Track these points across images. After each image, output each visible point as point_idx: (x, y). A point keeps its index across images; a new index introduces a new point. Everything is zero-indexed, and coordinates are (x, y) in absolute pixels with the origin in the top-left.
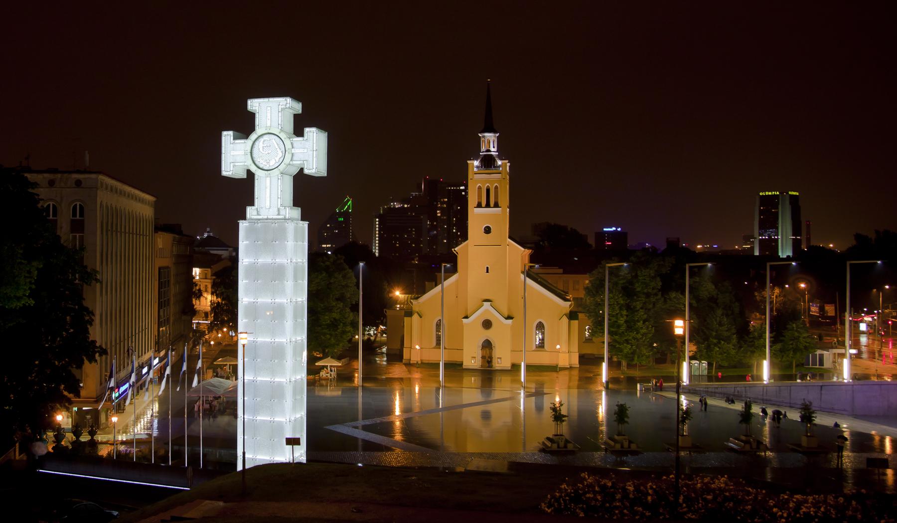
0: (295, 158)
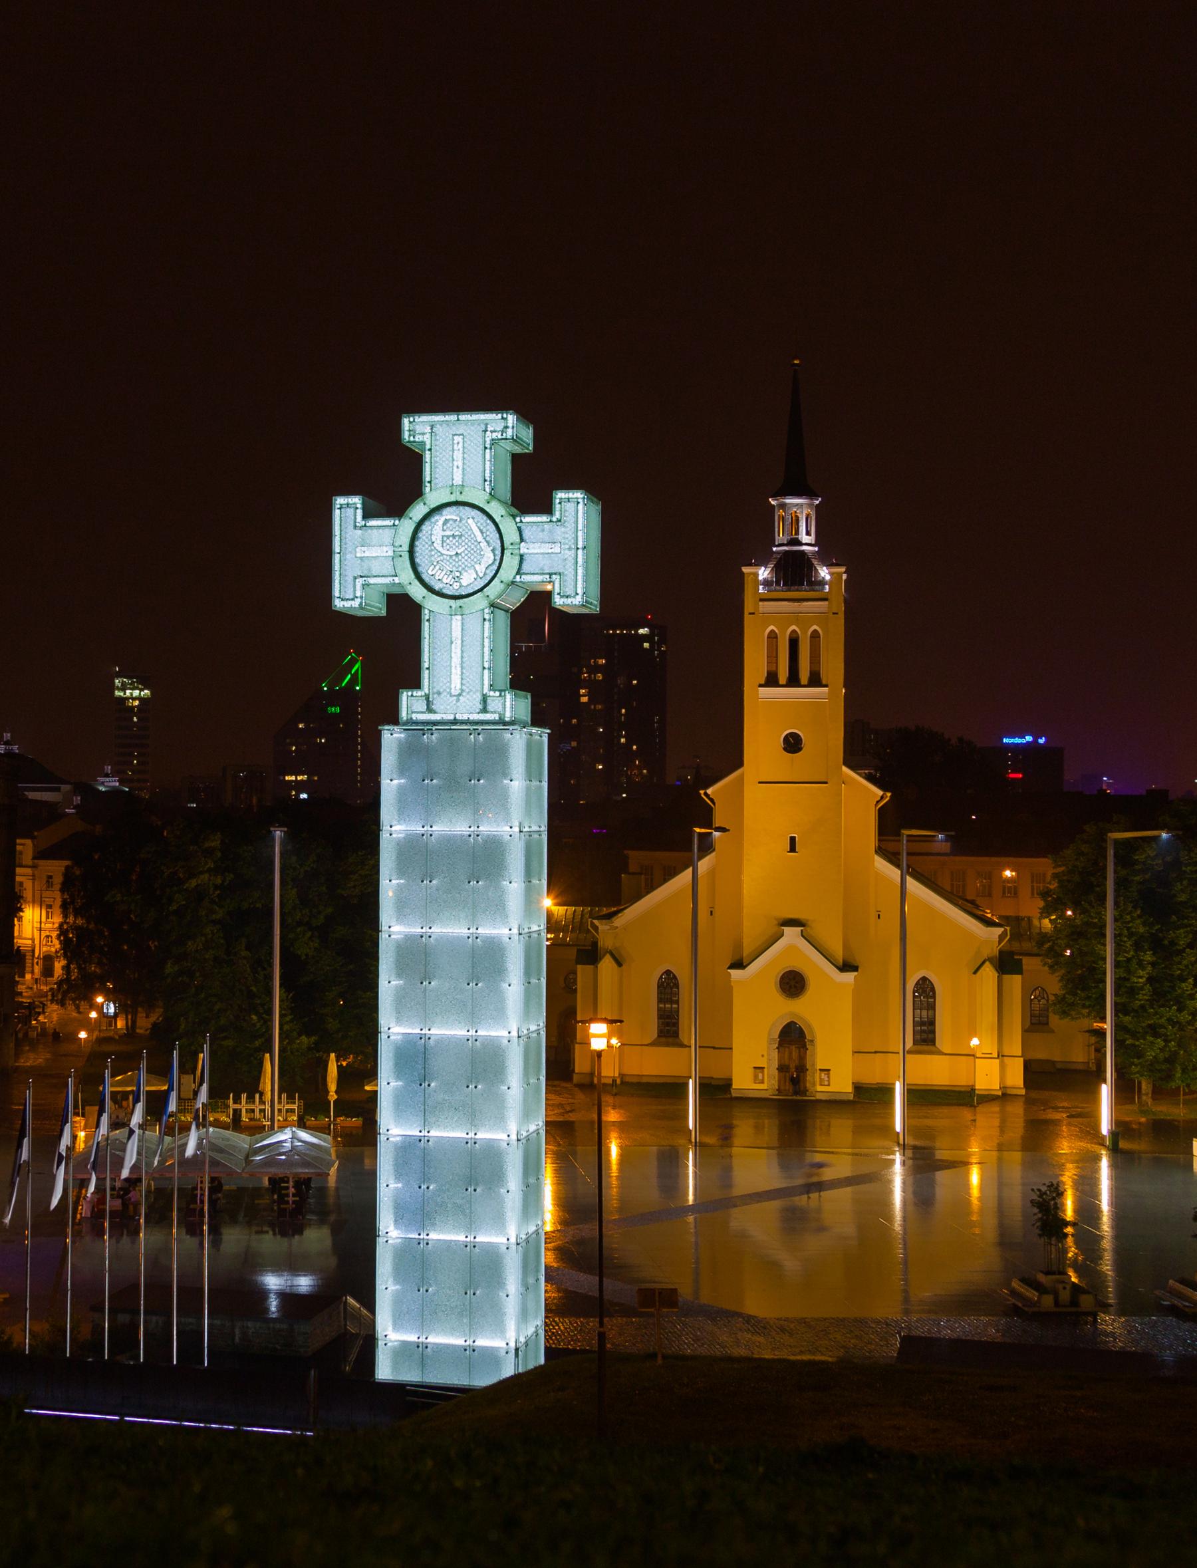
0: (526, 567)
